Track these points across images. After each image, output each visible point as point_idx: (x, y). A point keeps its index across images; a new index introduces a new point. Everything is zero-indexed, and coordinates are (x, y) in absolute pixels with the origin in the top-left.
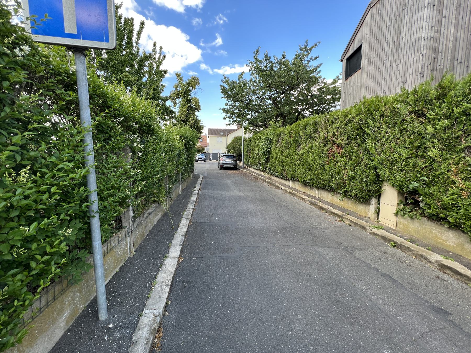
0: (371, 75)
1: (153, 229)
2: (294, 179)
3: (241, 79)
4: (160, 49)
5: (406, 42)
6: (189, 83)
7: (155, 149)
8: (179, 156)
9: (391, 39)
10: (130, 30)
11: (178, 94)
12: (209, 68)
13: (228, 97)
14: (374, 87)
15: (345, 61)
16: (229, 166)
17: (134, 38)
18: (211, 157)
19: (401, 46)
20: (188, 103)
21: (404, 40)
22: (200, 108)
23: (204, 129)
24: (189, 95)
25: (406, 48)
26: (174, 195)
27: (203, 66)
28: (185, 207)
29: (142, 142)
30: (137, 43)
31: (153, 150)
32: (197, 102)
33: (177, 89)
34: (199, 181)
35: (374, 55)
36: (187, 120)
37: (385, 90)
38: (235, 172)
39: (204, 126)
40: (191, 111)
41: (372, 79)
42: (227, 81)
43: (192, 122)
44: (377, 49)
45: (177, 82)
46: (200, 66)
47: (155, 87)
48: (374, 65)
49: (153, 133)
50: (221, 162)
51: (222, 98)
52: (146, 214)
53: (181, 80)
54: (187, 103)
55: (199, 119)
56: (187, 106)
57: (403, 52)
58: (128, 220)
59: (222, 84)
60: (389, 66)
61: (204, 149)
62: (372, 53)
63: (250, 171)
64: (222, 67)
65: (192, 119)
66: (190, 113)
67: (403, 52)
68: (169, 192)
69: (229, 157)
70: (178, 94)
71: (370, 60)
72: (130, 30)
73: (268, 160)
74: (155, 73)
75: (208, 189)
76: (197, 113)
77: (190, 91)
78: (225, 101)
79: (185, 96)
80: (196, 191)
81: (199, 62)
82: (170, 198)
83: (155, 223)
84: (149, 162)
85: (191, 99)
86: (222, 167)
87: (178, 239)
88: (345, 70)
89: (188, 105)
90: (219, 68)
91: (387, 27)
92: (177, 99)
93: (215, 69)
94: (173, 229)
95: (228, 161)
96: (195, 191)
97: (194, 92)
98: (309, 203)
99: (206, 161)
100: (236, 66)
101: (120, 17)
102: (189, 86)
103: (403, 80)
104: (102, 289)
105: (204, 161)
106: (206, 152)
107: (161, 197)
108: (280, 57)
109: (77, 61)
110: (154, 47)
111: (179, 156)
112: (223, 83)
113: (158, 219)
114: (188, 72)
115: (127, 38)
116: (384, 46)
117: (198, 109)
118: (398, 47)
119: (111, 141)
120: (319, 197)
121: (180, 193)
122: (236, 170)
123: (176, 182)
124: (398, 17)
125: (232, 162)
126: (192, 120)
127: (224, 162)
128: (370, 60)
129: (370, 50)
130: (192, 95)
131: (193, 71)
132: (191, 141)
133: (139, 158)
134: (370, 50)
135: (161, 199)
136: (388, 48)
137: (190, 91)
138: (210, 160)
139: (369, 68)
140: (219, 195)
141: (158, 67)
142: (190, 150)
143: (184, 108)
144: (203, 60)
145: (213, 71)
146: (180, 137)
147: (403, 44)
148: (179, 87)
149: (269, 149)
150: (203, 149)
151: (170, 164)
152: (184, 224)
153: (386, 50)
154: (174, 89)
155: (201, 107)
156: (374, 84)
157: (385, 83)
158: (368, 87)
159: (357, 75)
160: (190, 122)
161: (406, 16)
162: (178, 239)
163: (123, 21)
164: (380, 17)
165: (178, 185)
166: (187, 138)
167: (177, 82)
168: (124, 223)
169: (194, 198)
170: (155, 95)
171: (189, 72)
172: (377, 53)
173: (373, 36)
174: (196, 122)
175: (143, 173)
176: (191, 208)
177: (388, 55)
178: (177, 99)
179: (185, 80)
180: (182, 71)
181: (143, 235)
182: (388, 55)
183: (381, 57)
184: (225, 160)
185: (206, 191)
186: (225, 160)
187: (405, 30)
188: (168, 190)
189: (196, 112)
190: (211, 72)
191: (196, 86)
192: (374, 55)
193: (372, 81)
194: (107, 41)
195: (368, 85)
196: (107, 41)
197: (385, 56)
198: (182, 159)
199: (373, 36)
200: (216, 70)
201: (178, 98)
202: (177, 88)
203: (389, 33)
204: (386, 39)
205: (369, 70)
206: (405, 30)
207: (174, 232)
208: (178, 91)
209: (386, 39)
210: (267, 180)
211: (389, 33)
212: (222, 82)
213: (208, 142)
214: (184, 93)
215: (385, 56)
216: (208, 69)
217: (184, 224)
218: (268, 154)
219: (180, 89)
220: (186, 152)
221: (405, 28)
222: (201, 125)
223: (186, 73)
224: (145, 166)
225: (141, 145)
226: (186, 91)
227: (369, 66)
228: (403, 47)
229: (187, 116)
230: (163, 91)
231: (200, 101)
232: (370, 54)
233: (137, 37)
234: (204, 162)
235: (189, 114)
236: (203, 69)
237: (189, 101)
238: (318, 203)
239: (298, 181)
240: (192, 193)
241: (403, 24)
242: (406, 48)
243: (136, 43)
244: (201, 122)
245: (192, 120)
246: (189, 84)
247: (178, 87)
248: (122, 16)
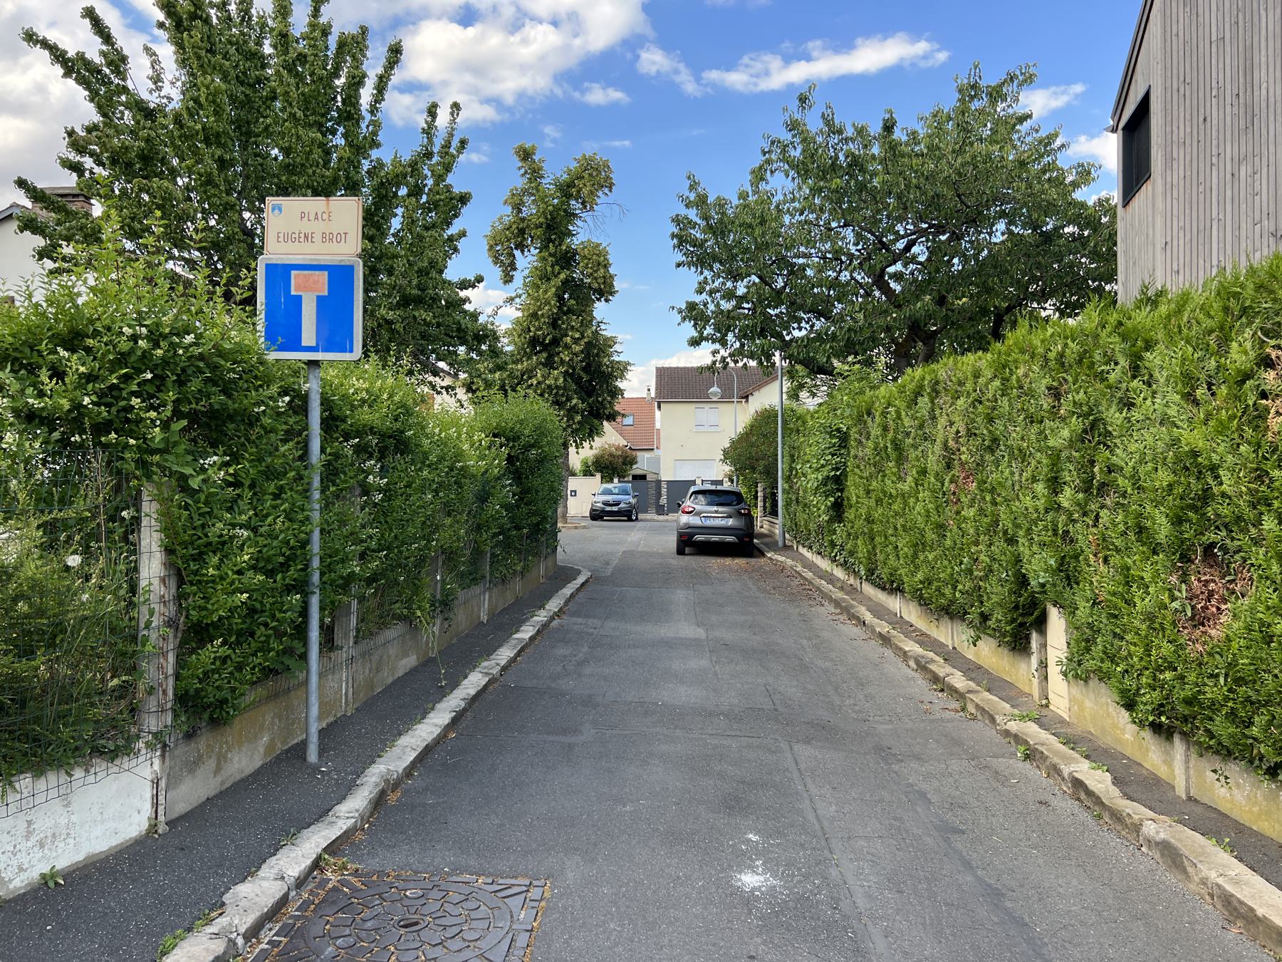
0: (1175, 202)
1: (394, 683)
2: (893, 586)
3: (762, 186)
4: (452, 114)
5: (1272, 100)
6: (570, 185)
7: (408, 486)
8: (483, 498)
9: (1228, 86)
10: (353, 78)
11: (522, 232)
12: (681, 66)
13: (701, 260)
14: (1188, 247)
15: (1120, 131)
16: (715, 538)
17: (366, 95)
18: (663, 500)
19: (1256, 111)
20: (562, 268)
21: (1264, 92)
22: (612, 286)
23: (629, 375)
24: (570, 234)
25: (1272, 118)
26: (461, 617)
27: (653, 60)
28: (489, 651)
29: (383, 472)
30: (373, 110)
31: (406, 487)
32: (599, 261)
33: (520, 211)
34: (568, 591)
35: (1182, 135)
36: (556, 342)
37: (1221, 259)
38: (740, 562)
39: (629, 364)
40: (573, 302)
41: (1182, 218)
42: (701, 201)
43: (577, 348)
44: (1188, 117)
45: (521, 182)
46: (637, 57)
47: (426, 264)
48: (1182, 168)
49: (406, 447)
50: (684, 519)
51: (679, 265)
52: (380, 639)
53: (535, 174)
54: (557, 268)
55: (607, 332)
56: (557, 282)
57: (1264, 132)
58: (346, 635)
59: (683, 211)
60: (1229, 176)
61: (633, 461)
62: (1175, 129)
63: (803, 560)
64: (746, 60)
65: (577, 335)
66: (570, 311)
67: (1264, 132)
68: (445, 604)
69: (721, 499)
70: (522, 232)
71: (1169, 149)
72: (353, 78)
73: (838, 509)
74: (428, 202)
75: (587, 616)
76: (600, 309)
77: (575, 215)
78: (692, 277)
79: (550, 240)
80: (541, 617)
81: (631, 45)
82: (446, 619)
83: (400, 673)
84: (395, 514)
85: (575, 253)
86: (689, 543)
87: (455, 700)
88: (1121, 169)
89: (562, 276)
90: (730, 66)
91: (1214, 45)
92: (517, 253)
93: (710, 68)
94: (441, 687)
95: (719, 518)
96: (535, 618)
97: (588, 219)
98: (915, 667)
99: (641, 516)
100: (814, 45)
101: (325, 32)
102: (569, 196)
103: (1272, 229)
104: (314, 729)
105: (627, 515)
106: (643, 477)
107: (419, 608)
108: (875, 128)
109: (311, 376)
110: (429, 119)
111: (483, 498)
112: (687, 206)
113: (409, 667)
114: (583, 92)
115: (344, 101)
116: (1208, 105)
117: (605, 290)
118: (1251, 114)
119: (340, 478)
120: (954, 648)
121: (484, 618)
122: (750, 555)
123: (472, 578)
124: (1240, 14)
125: (730, 522)
126: (576, 341)
127: (695, 521)
128: (1169, 149)
129: (1169, 118)
130: (583, 233)
131: (609, 83)
132: (533, 446)
133: (376, 505)
134: (1169, 118)
135: (419, 614)
136: (1221, 116)
137: (571, 216)
138: (660, 510)
139: (1169, 180)
140: (618, 634)
141: (439, 178)
142: (527, 478)
143: (546, 292)
144: (650, 32)
145: (698, 79)
146: (495, 436)
147: (1264, 105)
148: (528, 200)
149: (837, 469)
150: (629, 461)
151: (448, 521)
152: (474, 682)
153: (1215, 122)
154: (509, 210)
155: (617, 285)
156: (1188, 238)
157: (1221, 235)
158: (1169, 247)
159: (1145, 192)
160: (567, 347)
161: (1263, 12)
162: (455, 700)
163: (333, 41)
164: (1188, 10)
165: (476, 589)
166: (516, 438)
167: (521, 182)
168: (338, 641)
169: (526, 633)
170: (423, 290)
171: (588, 89)
172: (1188, 130)
173: (1175, 71)
174: (595, 346)
175: (383, 535)
176: (505, 654)
177: (1221, 137)
178: (517, 253)
179: (555, 171)
180: (558, 92)
181: (372, 687)
182: (1221, 137)
183: (1202, 143)
184: (698, 514)
185: (580, 620)
186: (698, 514)
187: (1263, 60)
188: (442, 596)
189: (597, 304)
190: (690, 87)
191: (600, 193)
192: (1182, 135)
193: (1181, 224)
194: (351, 351)
195: (1169, 239)
196: (351, 351)
197: (1214, 142)
198: (495, 507)
199: (1175, 71)
200: (714, 75)
201: (521, 247)
202: (518, 208)
203: (1221, 66)
204: (1214, 84)
205: (1169, 186)
206: (1263, 60)
207: (442, 693)
208: (523, 220)
209: (1214, 84)
210: (839, 595)
211: (1221, 66)
212: (682, 206)
213: (658, 425)
214: (549, 227)
215: (1214, 142)
216: (677, 72)
217: (474, 682)
218: (838, 490)
219: (530, 210)
220: (510, 485)
221: (1263, 52)
222: (616, 358)
223: (577, 95)
224: (386, 522)
225: (381, 479)
226: (553, 218)
227: (1169, 172)
228: (1264, 115)
229: (554, 324)
230: (456, 250)
231: (611, 259)
232: (1169, 129)
233: (375, 92)
234: (630, 520)
235: (565, 314)
236: (653, 70)
237: (567, 259)
238: (933, 661)
239: (902, 592)
240: (527, 619)
241: (1256, 39)
242: (1272, 118)
243: (372, 112)
244: (617, 347)
245: (576, 341)
246: (567, 190)
247: (522, 203)
248: (331, 26)
